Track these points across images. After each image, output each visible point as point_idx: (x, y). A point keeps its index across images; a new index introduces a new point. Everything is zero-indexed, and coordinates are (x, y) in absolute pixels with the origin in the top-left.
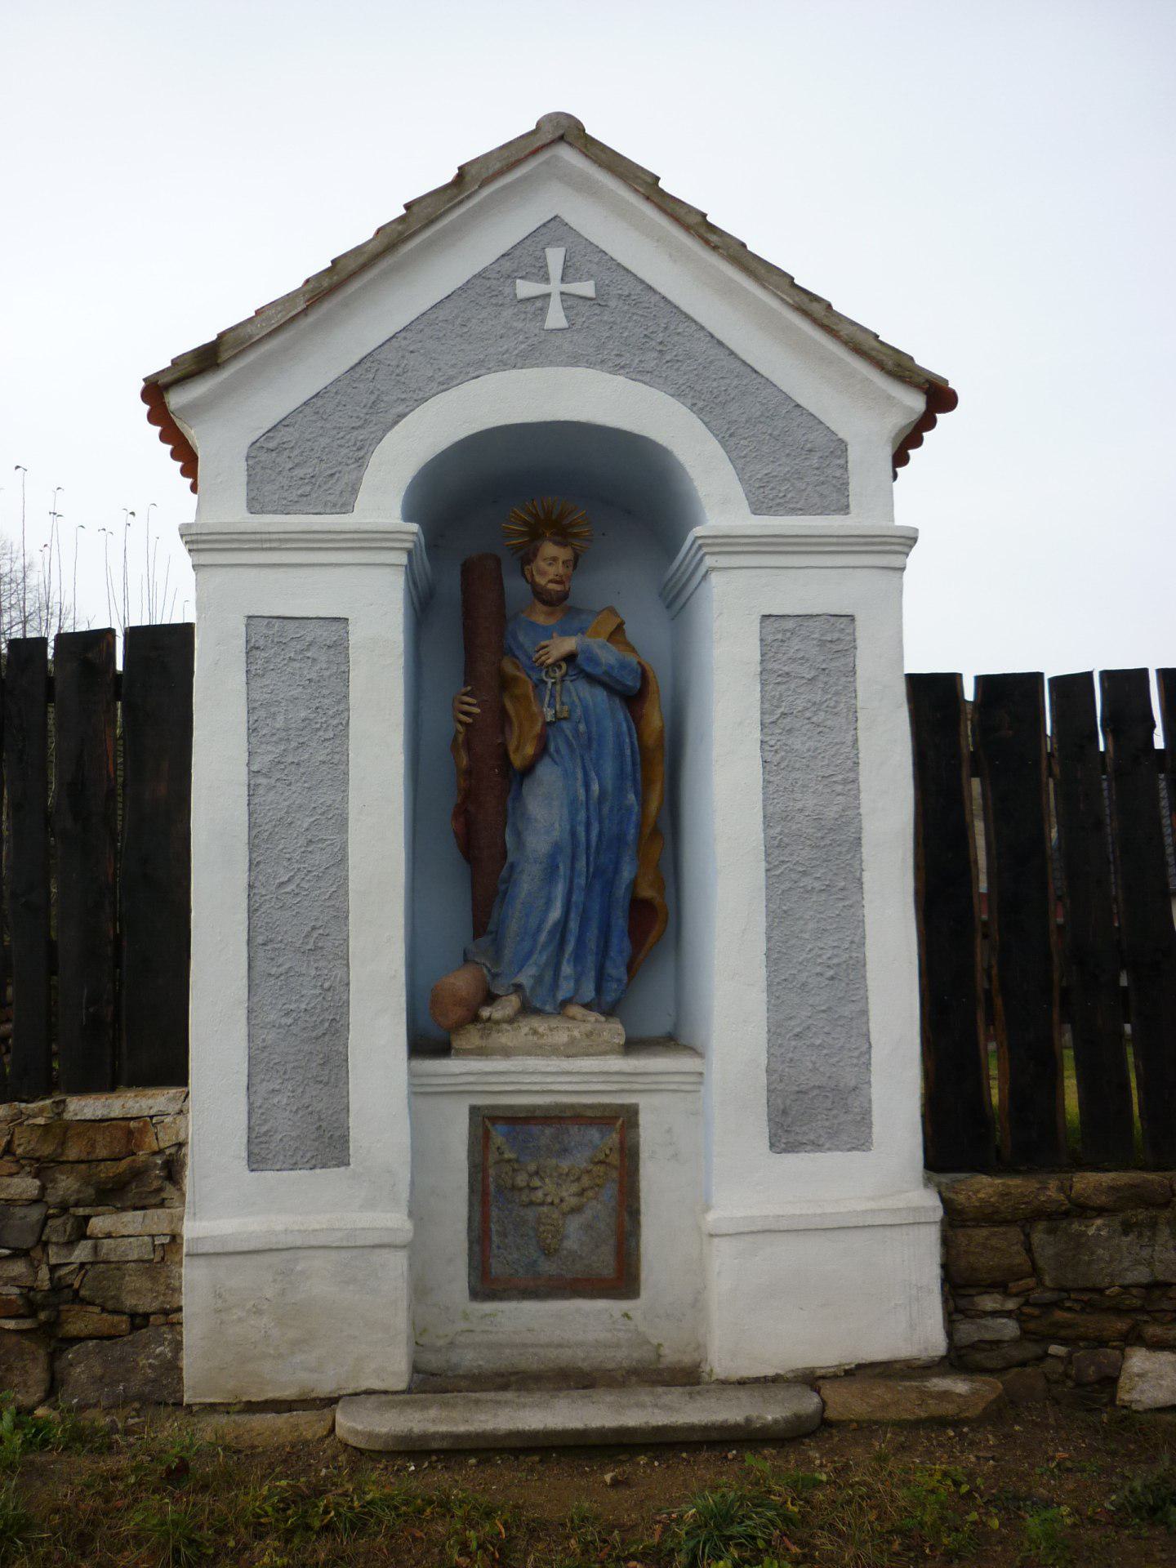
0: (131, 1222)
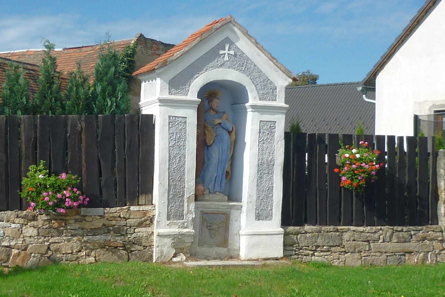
0: (143, 229)
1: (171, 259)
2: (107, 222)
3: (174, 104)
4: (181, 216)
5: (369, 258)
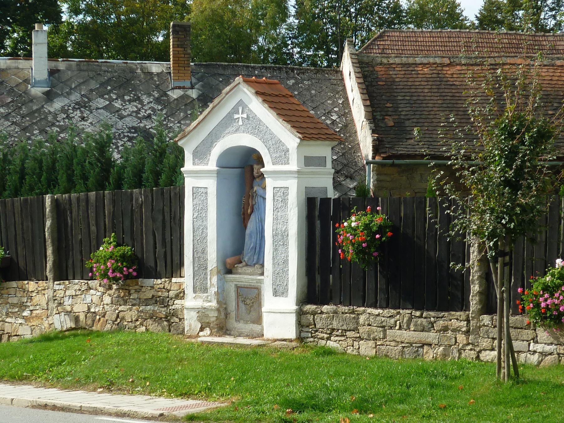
1: (198, 333)
2: (155, 294)
3: (196, 175)
4: (205, 290)
5: (383, 348)
